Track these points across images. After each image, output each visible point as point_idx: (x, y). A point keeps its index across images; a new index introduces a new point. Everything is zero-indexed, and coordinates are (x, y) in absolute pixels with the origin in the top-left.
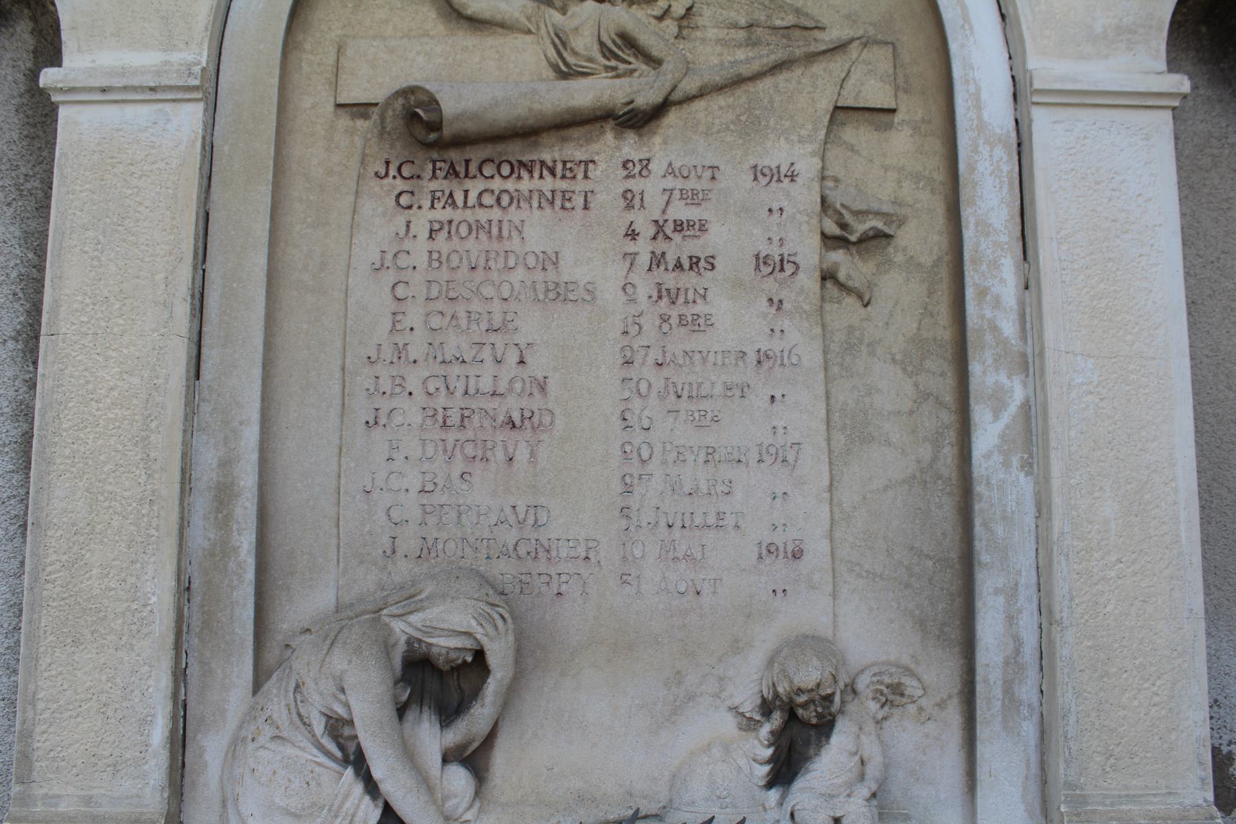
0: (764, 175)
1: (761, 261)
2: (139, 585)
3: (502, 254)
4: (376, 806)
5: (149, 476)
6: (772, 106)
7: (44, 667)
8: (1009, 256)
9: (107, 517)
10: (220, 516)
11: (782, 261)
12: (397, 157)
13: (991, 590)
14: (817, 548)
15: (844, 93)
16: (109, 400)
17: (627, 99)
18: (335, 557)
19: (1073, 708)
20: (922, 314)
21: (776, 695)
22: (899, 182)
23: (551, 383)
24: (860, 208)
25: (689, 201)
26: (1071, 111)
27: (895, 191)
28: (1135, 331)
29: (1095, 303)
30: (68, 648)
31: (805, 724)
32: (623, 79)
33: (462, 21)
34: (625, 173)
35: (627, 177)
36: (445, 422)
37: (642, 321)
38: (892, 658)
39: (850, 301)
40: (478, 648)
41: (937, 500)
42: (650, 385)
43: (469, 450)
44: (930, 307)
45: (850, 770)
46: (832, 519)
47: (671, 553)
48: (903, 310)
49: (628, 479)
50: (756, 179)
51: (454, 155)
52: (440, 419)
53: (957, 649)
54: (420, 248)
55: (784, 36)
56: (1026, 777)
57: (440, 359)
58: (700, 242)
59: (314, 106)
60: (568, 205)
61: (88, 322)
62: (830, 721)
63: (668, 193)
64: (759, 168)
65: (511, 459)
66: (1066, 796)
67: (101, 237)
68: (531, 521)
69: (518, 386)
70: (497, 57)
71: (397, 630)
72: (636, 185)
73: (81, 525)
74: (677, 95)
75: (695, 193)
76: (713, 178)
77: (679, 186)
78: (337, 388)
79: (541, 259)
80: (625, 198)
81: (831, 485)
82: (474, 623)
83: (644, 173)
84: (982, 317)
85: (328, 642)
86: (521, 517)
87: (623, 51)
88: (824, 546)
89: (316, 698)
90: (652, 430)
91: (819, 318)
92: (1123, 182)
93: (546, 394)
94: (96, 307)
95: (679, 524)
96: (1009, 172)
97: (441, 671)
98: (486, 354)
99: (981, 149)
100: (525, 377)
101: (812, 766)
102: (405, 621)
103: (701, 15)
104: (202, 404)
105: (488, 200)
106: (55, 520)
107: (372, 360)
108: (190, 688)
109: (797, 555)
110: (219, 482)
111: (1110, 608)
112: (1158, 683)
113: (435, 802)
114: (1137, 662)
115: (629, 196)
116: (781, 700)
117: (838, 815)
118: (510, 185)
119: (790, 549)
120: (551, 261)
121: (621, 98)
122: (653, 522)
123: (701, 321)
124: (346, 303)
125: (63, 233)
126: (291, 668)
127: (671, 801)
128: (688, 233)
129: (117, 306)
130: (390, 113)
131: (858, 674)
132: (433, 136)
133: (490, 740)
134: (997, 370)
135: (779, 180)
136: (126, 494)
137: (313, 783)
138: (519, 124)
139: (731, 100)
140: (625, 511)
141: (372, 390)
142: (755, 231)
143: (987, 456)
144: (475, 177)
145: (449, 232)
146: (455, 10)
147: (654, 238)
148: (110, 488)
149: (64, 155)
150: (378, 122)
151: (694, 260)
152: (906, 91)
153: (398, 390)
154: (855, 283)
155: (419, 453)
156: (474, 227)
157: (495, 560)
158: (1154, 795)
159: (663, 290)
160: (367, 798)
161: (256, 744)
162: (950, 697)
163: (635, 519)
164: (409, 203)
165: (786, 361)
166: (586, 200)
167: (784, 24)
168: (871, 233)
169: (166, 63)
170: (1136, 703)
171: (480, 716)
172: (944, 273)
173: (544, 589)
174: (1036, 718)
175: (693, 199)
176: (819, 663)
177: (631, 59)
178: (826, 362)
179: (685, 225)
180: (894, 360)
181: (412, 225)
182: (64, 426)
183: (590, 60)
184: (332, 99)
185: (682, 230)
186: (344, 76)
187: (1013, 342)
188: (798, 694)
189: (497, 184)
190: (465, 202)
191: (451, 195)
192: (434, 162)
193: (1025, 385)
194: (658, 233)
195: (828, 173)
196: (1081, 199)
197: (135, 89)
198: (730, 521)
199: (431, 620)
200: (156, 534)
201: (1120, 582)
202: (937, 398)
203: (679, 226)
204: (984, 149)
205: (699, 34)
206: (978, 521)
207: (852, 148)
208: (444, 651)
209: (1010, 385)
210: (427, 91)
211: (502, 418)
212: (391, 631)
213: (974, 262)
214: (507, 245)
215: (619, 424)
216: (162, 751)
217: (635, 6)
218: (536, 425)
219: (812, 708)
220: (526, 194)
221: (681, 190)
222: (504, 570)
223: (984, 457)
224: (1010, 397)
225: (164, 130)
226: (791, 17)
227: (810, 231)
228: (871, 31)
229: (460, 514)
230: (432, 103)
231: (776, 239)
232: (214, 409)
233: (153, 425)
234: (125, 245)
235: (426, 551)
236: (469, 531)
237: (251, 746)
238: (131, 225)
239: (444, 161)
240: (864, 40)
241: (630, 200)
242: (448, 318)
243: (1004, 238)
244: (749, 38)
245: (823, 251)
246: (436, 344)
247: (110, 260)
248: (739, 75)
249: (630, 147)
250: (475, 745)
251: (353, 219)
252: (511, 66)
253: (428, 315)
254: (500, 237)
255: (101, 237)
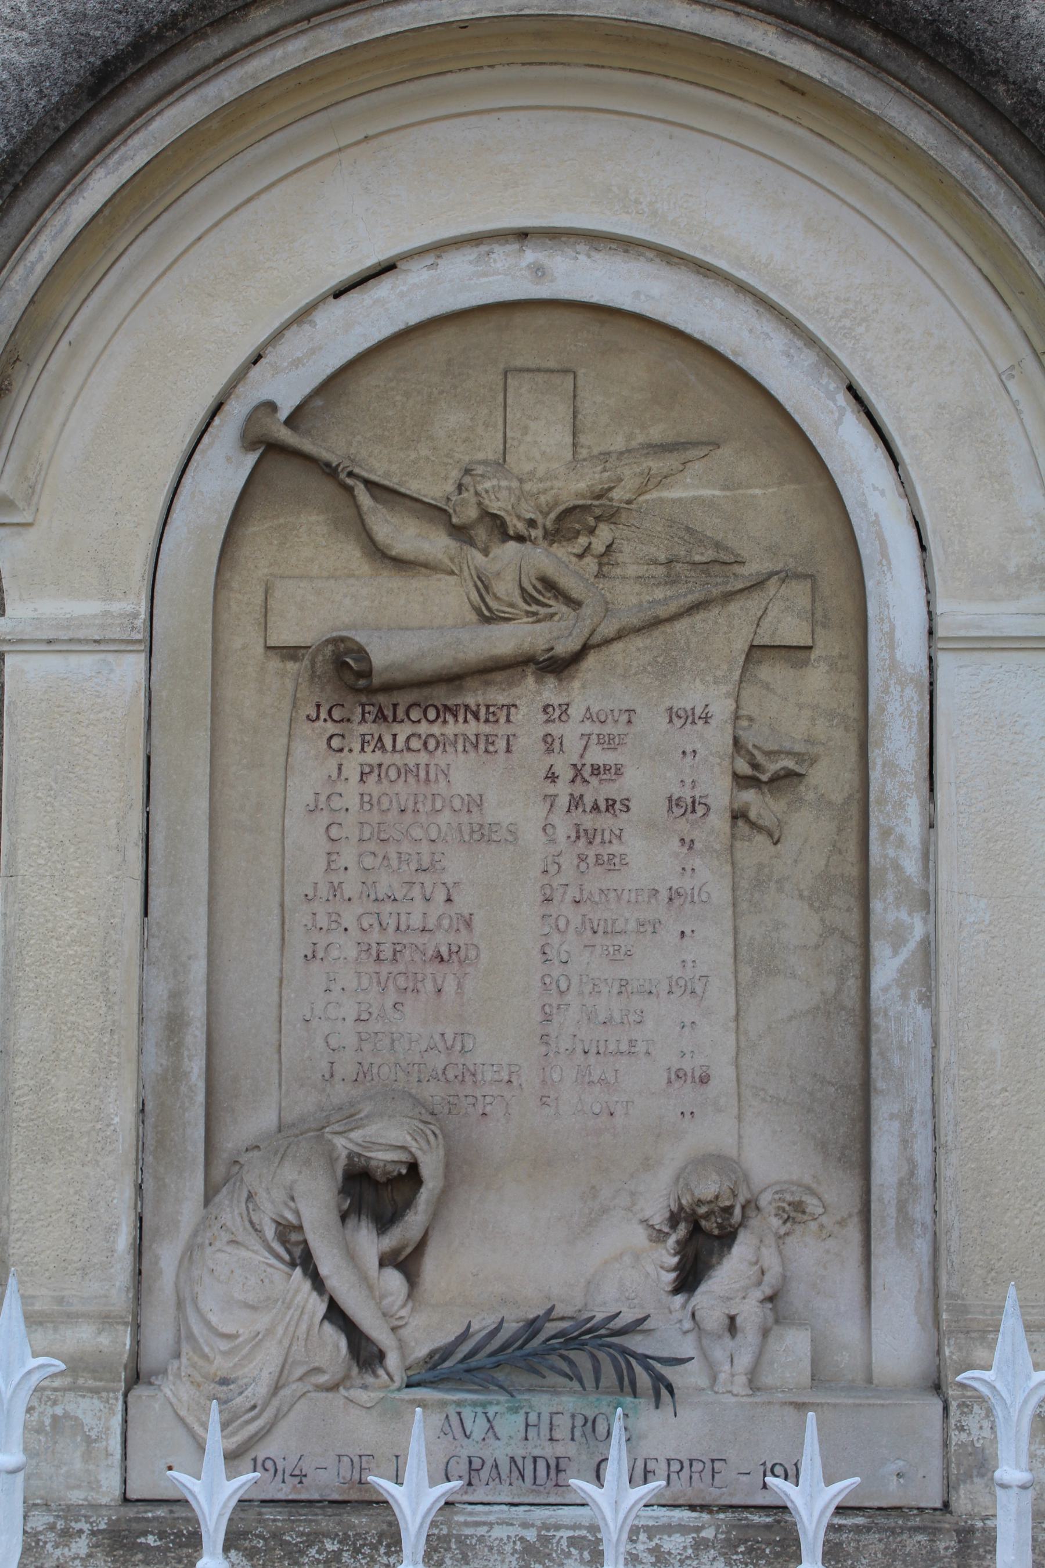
0: (679, 717)
1: (673, 802)
2: (102, 1107)
3: (430, 797)
4: (323, 1301)
5: (109, 1007)
6: (688, 648)
7: (16, 1182)
8: (915, 795)
9: (70, 1045)
10: (171, 1043)
11: (693, 802)
12: (327, 700)
13: (886, 1115)
14: (724, 1075)
15: (760, 631)
16: (68, 938)
17: (547, 646)
18: (277, 1081)
19: (956, 1224)
20: (830, 851)
21: (681, 1208)
22: (813, 719)
23: (476, 918)
24: (771, 748)
25: (605, 746)
26: (977, 655)
27: (808, 730)
28: (1028, 872)
29: (991, 845)
30: (37, 1164)
31: (709, 1235)
32: (543, 624)
33: (386, 561)
34: (546, 717)
35: (547, 721)
36: (378, 956)
37: (561, 860)
38: (795, 1178)
39: (760, 839)
40: (412, 1161)
41: (840, 1029)
42: (568, 922)
43: (402, 982)
44: (838, 845)
45: (749, 1278)
46: (738, 1047)
47: (587, 1077)
48: (811, 848)
49: (547, 1009)
50: (671, 721)
51: (382, 699)
52: (374, 952)
53: (857, 1171)
54: (351, 791)
55: (703, 572)
56: (919, 1291)
57: (373, 897)
58: (617, 785)
59: (244, 647)
60: (491, 748)
61: (46, 865)
62: (731, 1232)
63: (586, 738)
64: (675, 710)
65: (439, 991)
66: (948, 1305)
67: (53, 784)
68: (458, 1047)
69: (446, 922)
70: (421, 599)
71: (340, 1146)
72: (555, 729)
73: (47, 1053)
74: (597, 638)
75: (611, 738)
76: (629, 722)
77: (596, 731)
78: (276, 923)
79: (466, 802)
80: (546, 742)
81: (737, 1014)
82: (409, 1138)
83: (564, 718)
84: (885, 856)
85: (279, 1156)
86: (450, 1043)
87: (543, 595)
88: (730, 1072)
89: (267, 1206)
90: (569, 965)
91: (729, 856)
92: (1026, 725)
93: (471, 930)
94: (52, 851)
95: (594, 1050)
96: (918, 712)
97: (377, 1183)
98: (416, 892)
99: (892, 689)
100: (453, 914)
101: (713, 1273)
102: (347, 1138)
103: (621, 552)
104: (151, 940)
105: (415, 744)
106: (22, 1049)
107: (309, 897)
108: (146, 1201)
109: (704, 1080)
110: (169, 1013)
111: (994, 1133)
112: (1040, 1204)
113: (374, 1298)
114: (1020, 1184)
115: (549, 740)
116: (686, 1212)
117: (733, 1313)
118: (436, 729)
119: (697, 1075)
120: (475, 803)
121: (541, 645)
122: (571, 1049)
123: (617, 860)
124: (283, 843)
125: (17, 779)
126: (242, 1180)
127: (586, 1305)
128: (605, 777)
129: (72, 850)
130: (320, 658)
131: (761, 1192)
132: (362, 683)
133: (421, 1246)
134: (898, 907)
135: (693, 722)
136: (88, 1024)
137: (266, 1281)
138: (444, 672)
139: (649, 641)
140: (544, 1038)
141: (310, 926)
142: (668, 775)
143: (885, 990)
144: (402, 721)
145: (379, 775)
146: (378, 549)
147: (573, 781)
148: (73, 1019)
149: (12, 703)
150: (309, 666)
151: (610, 802)
152: (824, 626)
153: (334, 926)
154: (767, 821)
155: (355, 984)
156: (403, 771)
157: (425, 1083)
158: (1033, 1307)
159: (581, 831)
160: (315, 1294)
161: (213, 1248)
162: (850, 1216)
163: (553, 1046)
164: (341, 746)
165: (696, 898)
166: (508, 743)
167: (704, 559)
168: (782, 773)
169: (106, 613)
170: (1017, 1222)
171: (415, 1221)
172: (854, 810)
173: (470, 1109)
174: (929, 1236)
175: (609, 743)
176: (717, 1177)
177: (551, 602)
178: (734, 898)
179: (602, 769)
180: (801, 896)
181: (343, 768)
182: (27, 962)
183: (512, 605)
184: (262, 641)
185: (599, 773)
186: (273, 619)
187: (915, 880)
188: (698, 1205)
189: (423, 728)
190: (394, 746)
191: (380, 739)
192: (363, 706)
193: (925, 921)
194: (576, 776)
195: (742, 712)
196: (984, 743)
197: (79, 641)
198: (641, 1047)
199: (370, 1136)
200: (117, 1060)
201: (1005, 1109)
202: (843, 932)
203: (596, 770)
204: (895, 690)
205: (618, 571)
206: (874, 1051)
207: (767, 687)
208: (381, 1164)
209: (910, 921)
210: (357, 643)
211: (431, 953)
212: (334, 1145)
213: (879, 802)
214: (434, 788)
215: (538, 957)
216: (127, 1256)
217: (555, 545)
218: (462, 959)
219: (713, 1219)
220: (452, 738)
221: (598, 735)
222: (433, 1092)
223: (882, 990)
224: (911, 934)
225: (108, 680)
226: (710, 552)
227: (722, 773)
228: (792, 564)
229: (393, 1041)
230: (361, 653)
231: (688, 781)
232: (163, 945)
233: (111, 961)
234: (76, 791)
235: (361, 1075)
236: (402, 1056)
237: (209, 1250)
238: (82, 772)
239: (373, 705)
240: (783, 575)
241: (549, 743)
242: (380, 859)
243: (910, 779)
244: (668, 575)
245: (735, 791)
246: (369, 882)
247: (63, 806)
248: (657, 617)
249: (550, 692)
250: (409, 1250)
251: (287, 761)
252: (436, 609)
253: (360, 855)
254: (427, 780)
255: (53, 784)
